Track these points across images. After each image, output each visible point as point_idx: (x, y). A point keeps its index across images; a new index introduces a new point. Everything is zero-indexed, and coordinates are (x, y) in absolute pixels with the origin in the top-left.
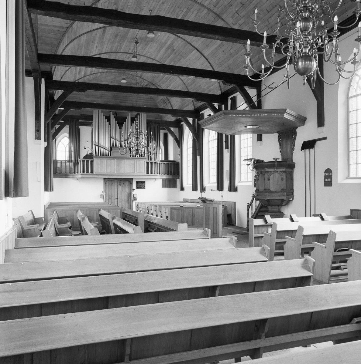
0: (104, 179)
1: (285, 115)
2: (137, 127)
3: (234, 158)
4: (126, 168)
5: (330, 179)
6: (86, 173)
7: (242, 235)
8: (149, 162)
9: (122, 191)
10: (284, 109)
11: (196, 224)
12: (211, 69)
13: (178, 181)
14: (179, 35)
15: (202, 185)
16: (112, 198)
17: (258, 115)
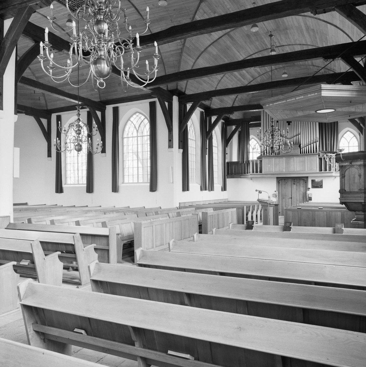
0: (277, 178)
2: (272, 124)
4: (295, 166)
6: (327, 171)
9: (296, 191)
14: (303, 14)
17: (294, 99)
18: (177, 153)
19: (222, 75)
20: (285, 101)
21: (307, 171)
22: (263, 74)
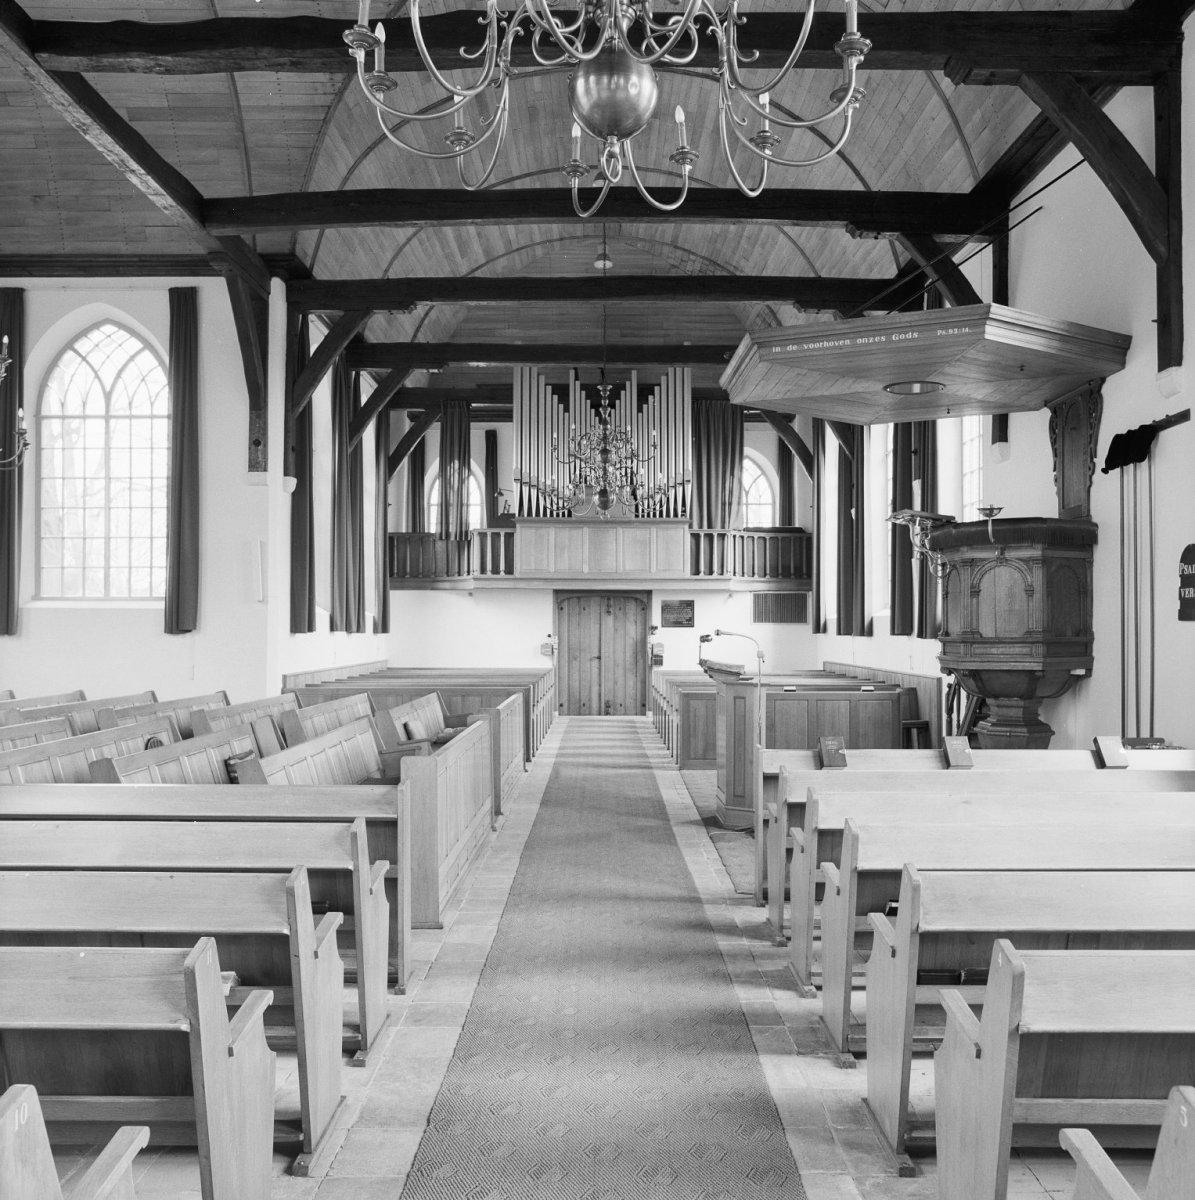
0: (556, 592)
1: (988, 329)
8: (702, 534)
9: (615, 634)
12: (858, 187)
16: (583, 654)
18: (279, 487)
19: (410, 231)
20: (848, 342)
21: (654, 573)
22: (518, 249)
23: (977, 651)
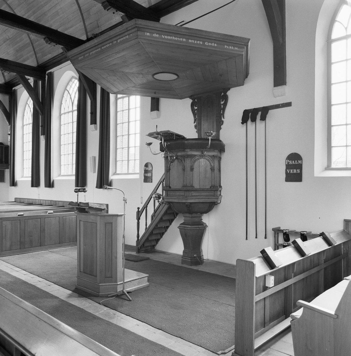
3: (107, 139)
5: (299, 171)
7: (136, 263)
10: (246, 39)
11: (46, 244)
13: (7, 173)
15: (48, 176)
23: (193, 194)
